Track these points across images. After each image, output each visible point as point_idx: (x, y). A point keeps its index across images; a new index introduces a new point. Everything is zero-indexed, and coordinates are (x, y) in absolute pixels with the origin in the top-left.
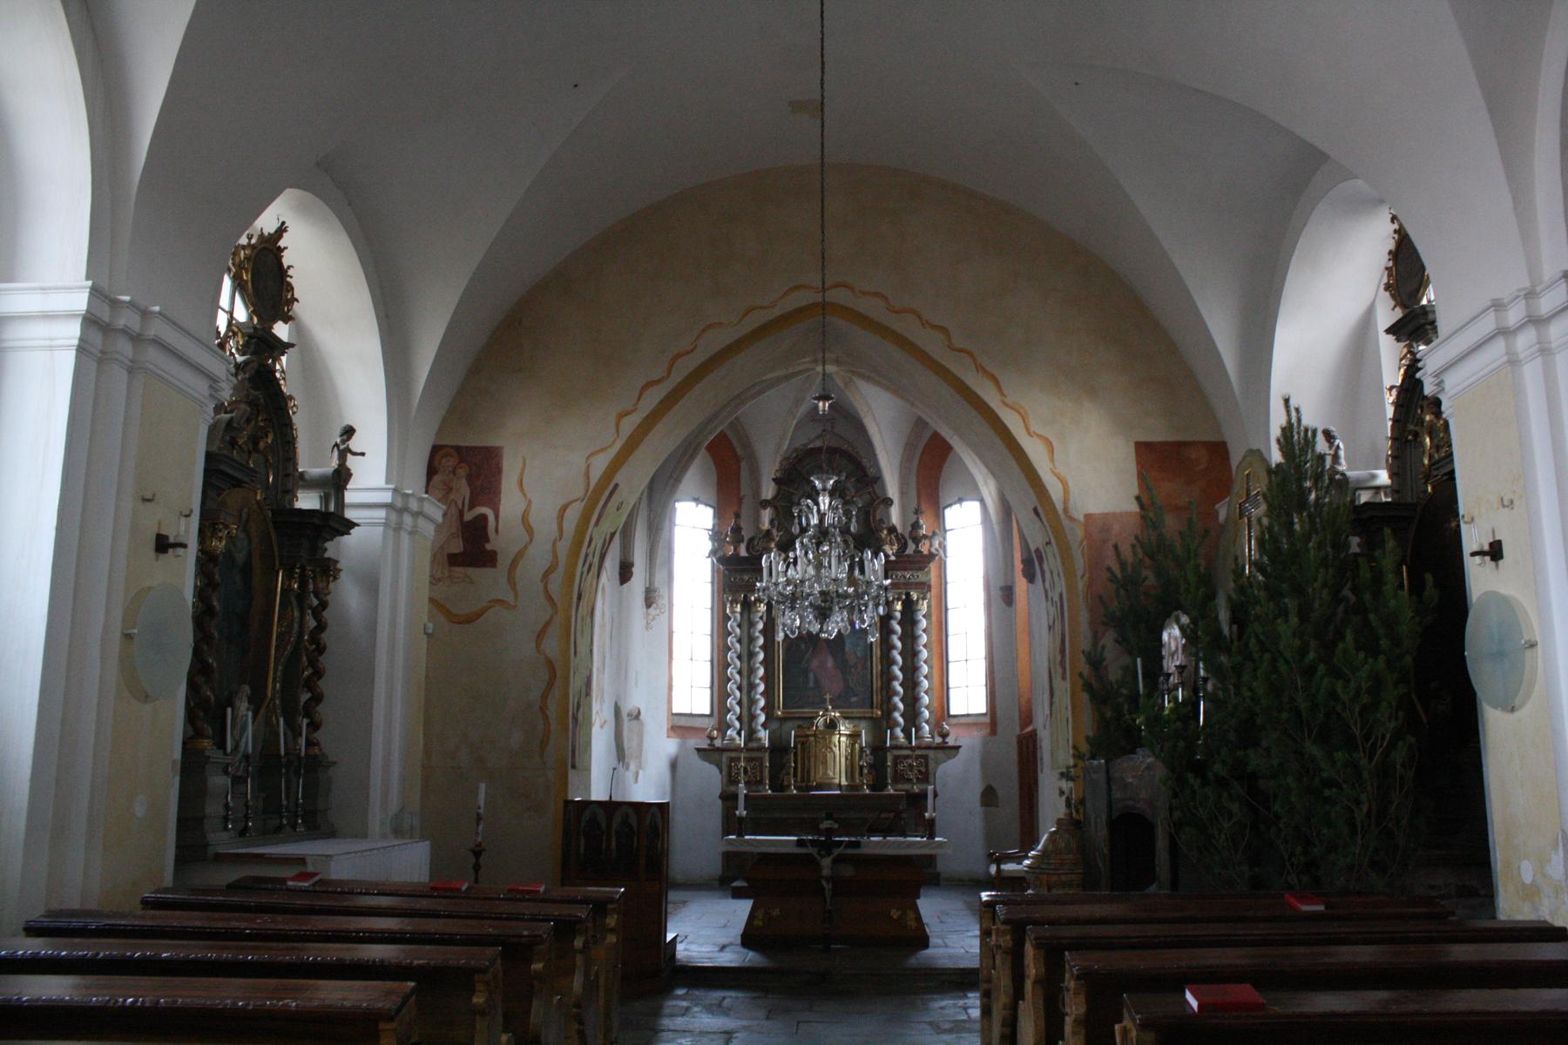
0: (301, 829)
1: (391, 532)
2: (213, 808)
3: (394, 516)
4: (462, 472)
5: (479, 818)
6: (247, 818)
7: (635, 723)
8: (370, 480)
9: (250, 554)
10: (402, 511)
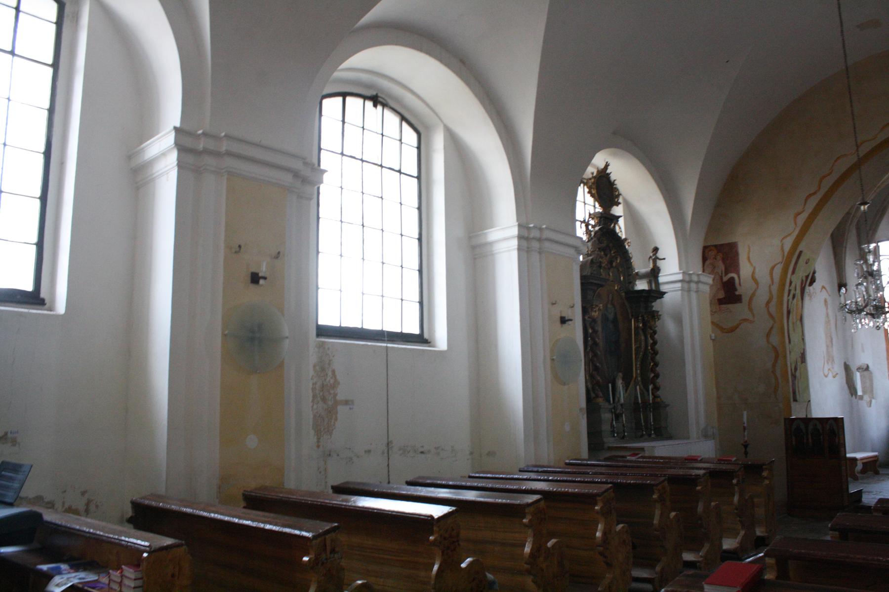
0: (653, 436)
1: (686, 293)
2: (606, 427)
3: (686, 285)
4: (719, 257)
5: (745, 429)
6: (624, 431)
7: (866, 373)
8: (671, 269)
9: (616, 314)
10: (689, 282)
